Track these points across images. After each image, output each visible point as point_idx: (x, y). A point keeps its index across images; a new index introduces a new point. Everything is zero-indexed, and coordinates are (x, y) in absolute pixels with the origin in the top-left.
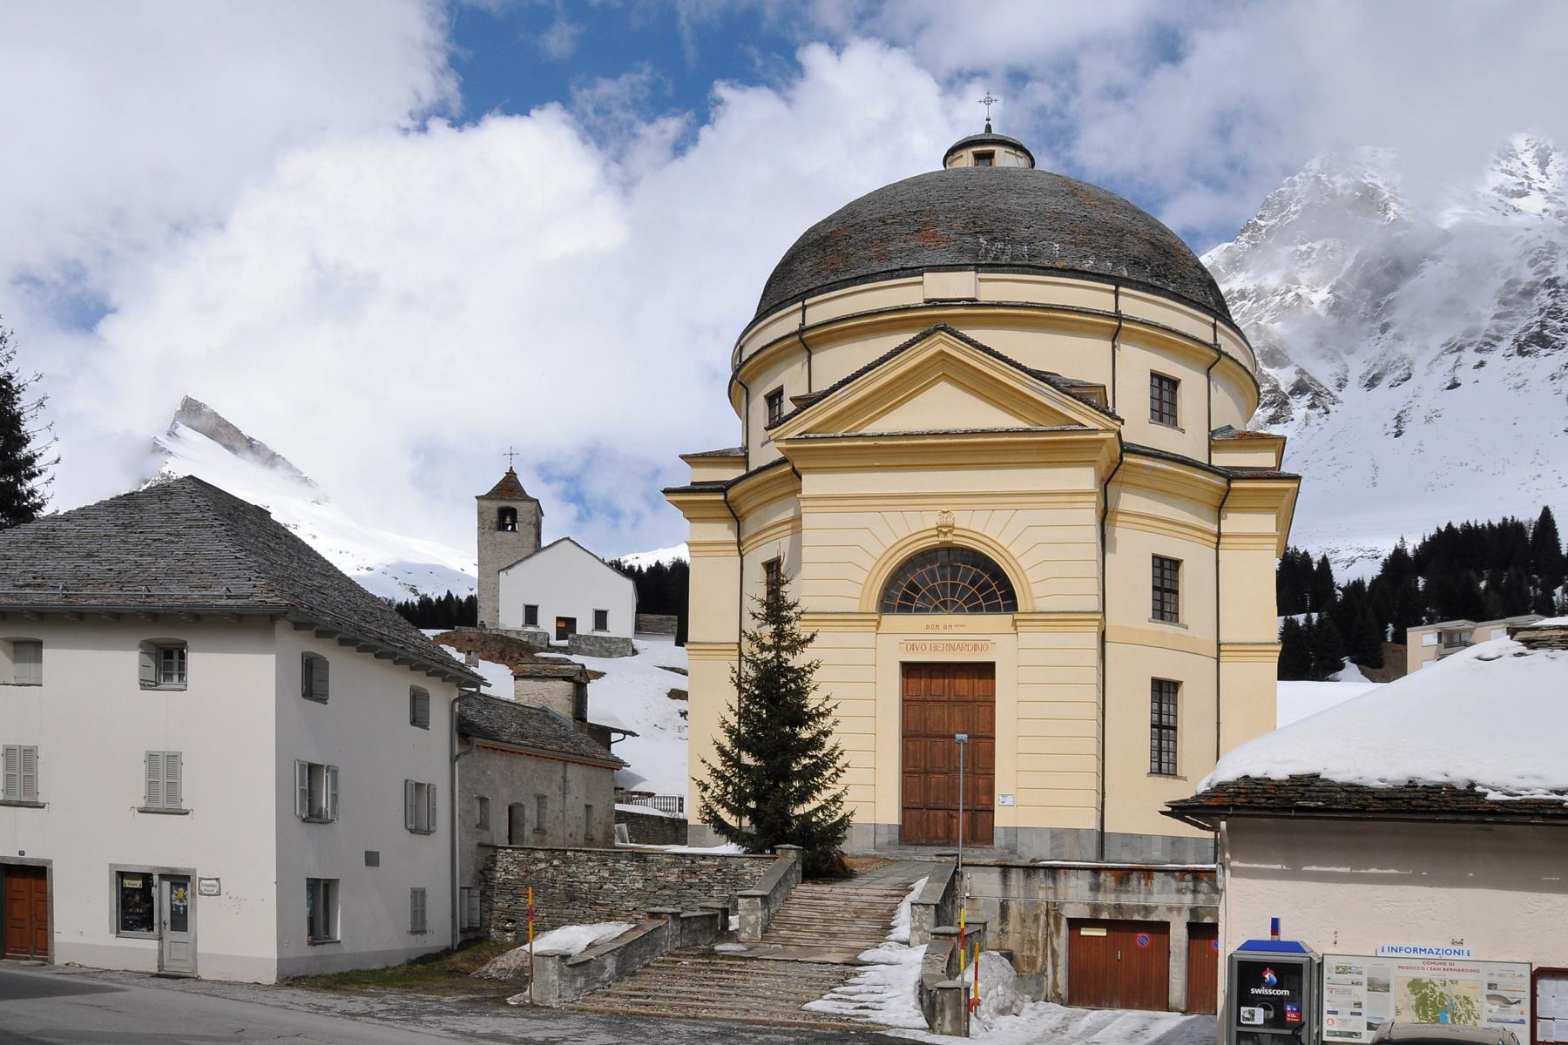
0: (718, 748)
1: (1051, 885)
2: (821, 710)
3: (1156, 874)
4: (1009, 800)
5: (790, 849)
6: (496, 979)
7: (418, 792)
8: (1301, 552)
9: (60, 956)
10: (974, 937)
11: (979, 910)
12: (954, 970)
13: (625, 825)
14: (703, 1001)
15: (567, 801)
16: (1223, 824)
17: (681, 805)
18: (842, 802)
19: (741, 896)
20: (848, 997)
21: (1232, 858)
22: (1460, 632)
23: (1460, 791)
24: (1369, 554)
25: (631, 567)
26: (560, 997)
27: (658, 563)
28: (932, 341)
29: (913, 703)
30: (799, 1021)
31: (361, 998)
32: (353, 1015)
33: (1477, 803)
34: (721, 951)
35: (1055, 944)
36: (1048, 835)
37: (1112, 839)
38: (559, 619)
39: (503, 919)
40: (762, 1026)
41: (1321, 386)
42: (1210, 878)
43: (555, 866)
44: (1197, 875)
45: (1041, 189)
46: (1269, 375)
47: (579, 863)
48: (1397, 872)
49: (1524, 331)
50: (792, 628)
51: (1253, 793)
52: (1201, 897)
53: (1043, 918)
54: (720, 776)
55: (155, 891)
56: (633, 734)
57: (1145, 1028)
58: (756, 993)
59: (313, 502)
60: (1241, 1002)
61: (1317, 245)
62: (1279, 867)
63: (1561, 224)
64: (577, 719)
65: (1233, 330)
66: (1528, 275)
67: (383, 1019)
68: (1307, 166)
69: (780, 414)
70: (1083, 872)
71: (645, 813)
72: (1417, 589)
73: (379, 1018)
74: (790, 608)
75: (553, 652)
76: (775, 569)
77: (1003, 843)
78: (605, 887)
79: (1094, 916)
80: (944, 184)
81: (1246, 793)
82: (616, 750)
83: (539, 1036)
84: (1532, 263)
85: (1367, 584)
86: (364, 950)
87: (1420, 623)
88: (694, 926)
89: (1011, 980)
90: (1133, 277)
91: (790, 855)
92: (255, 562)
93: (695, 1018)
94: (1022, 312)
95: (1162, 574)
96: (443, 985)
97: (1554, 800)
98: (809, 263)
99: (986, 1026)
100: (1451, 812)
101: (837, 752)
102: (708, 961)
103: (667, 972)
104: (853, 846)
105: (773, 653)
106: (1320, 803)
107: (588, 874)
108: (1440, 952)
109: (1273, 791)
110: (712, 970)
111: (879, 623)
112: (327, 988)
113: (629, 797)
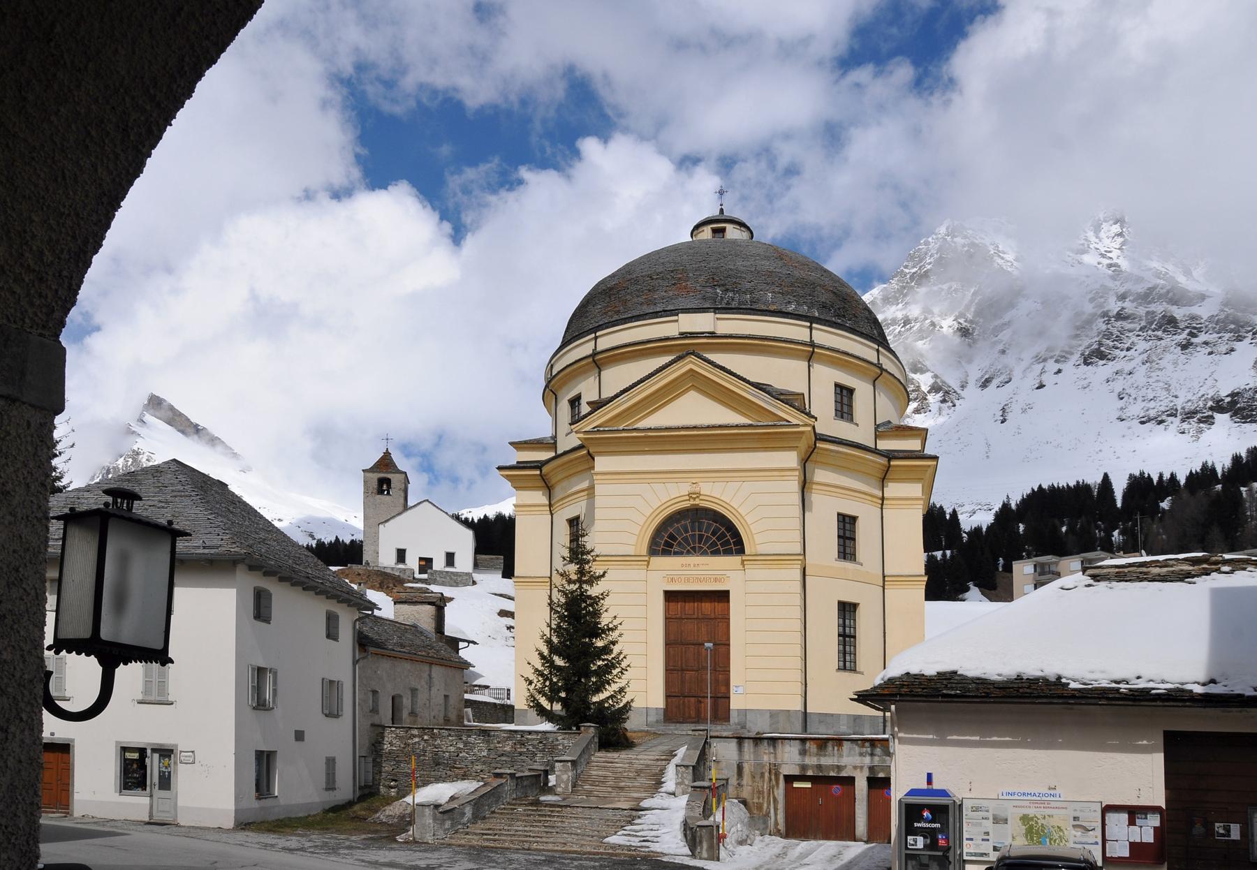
0: (539, 654)
1: (772, 751)
2: (611, 626)
3: (845, 743)
4: (740, 690)
5: (590, 726)
6: (385, 823)
7: (331, 687)
8: (938, 506)
9: (78, 810)
10: (720, 789)
11: (722, 770)
12: (707, 813)
13: (470, 709)
14: (534, 837)
15: (432, 692)
16: (893, 707)
17: (509, 694)
18: (625, 692)
19: (557, 761)
20: (634, 833)
21: (899, 731)
22: (1049, 564)
23: (1051, 682)
24: (985, 507)
25: (466, 519)
26: (434, 835)
27: (485, 516)
28: (685, 362)
29: (672, 620)
30: (601, 850)
31: (294, 838)
32: (291, 850)
33: (1063, 690)
34: (545, 801)
35: (776, 793)
36: (768, 715)
37: (812, 716)
38: (421, 559)
39: (389, 779)
40: (575, 855)
41: (950, 387)
42: (882, 745)
43: (426, 740)
44: (873, 742)
45: (759, 255)
46: (913, 379)
47: (442, 737)
48: (1011, 739)
49: (1088, 348)
50: (590, 567)
51: (913, 685)
52: (876, 758)
53: (767, 775)
54: (541, 674)
55: (148, 761)
56: (474, 643)
57: (840, 853)
58: (570, 831)
59: (240, 471)
60: (907, 835)
61: (945, 287)
62: (978, 738)
63: (1110, 272)
64: (438, 633)
65: (891, 353)
66: (1089, 308)
67: (312, 852)
68: (937, 231)
69: (579, 413)
70: (794, 741)
71: (484, 700)
72: (1019, 532)
73: (310, 852)
74: (589, 553)
75: (417, 583)
76: (575, 523)
77: (736, 721)
78: (461, 755)
79: (803, 773)
80: (692, 251)
81: (908, 685)
82: (463, 654)
83: (422, 864)
84: (1092, 300)
85: (984, 529)
86: (293, 802)
87: (1021, 558)
88: (525, 783)
89: (746, 820)
90: (822, 317)
91: (590, 731)
92: (221, 522)
93: (529, 849)
94: (746, 341)
95: (844, 526)
96: (348, 828)
97: (1114, 688)
98: (600, 306)
99: (730, 853)
100: (1046, 697)
101: (622, 656)
102: (535, 808)
103: (508, 816)
104: (633, 724)
105: (577, 585)
106: (958, 692)
107: (449, 745)
108: (1041, 795)
109: (926, 683)
110: (539, 815)
111: (649, 562)
112: (269, 831)
113: (473, 689)
